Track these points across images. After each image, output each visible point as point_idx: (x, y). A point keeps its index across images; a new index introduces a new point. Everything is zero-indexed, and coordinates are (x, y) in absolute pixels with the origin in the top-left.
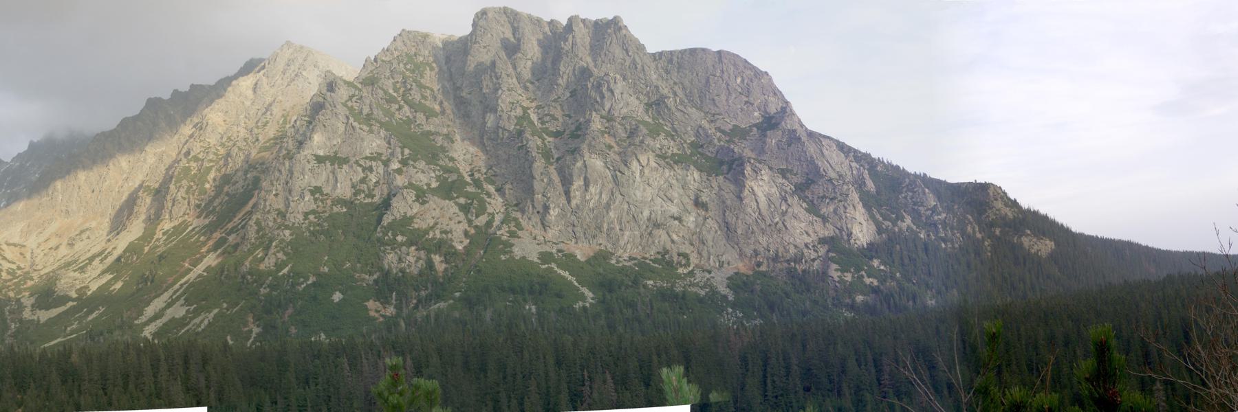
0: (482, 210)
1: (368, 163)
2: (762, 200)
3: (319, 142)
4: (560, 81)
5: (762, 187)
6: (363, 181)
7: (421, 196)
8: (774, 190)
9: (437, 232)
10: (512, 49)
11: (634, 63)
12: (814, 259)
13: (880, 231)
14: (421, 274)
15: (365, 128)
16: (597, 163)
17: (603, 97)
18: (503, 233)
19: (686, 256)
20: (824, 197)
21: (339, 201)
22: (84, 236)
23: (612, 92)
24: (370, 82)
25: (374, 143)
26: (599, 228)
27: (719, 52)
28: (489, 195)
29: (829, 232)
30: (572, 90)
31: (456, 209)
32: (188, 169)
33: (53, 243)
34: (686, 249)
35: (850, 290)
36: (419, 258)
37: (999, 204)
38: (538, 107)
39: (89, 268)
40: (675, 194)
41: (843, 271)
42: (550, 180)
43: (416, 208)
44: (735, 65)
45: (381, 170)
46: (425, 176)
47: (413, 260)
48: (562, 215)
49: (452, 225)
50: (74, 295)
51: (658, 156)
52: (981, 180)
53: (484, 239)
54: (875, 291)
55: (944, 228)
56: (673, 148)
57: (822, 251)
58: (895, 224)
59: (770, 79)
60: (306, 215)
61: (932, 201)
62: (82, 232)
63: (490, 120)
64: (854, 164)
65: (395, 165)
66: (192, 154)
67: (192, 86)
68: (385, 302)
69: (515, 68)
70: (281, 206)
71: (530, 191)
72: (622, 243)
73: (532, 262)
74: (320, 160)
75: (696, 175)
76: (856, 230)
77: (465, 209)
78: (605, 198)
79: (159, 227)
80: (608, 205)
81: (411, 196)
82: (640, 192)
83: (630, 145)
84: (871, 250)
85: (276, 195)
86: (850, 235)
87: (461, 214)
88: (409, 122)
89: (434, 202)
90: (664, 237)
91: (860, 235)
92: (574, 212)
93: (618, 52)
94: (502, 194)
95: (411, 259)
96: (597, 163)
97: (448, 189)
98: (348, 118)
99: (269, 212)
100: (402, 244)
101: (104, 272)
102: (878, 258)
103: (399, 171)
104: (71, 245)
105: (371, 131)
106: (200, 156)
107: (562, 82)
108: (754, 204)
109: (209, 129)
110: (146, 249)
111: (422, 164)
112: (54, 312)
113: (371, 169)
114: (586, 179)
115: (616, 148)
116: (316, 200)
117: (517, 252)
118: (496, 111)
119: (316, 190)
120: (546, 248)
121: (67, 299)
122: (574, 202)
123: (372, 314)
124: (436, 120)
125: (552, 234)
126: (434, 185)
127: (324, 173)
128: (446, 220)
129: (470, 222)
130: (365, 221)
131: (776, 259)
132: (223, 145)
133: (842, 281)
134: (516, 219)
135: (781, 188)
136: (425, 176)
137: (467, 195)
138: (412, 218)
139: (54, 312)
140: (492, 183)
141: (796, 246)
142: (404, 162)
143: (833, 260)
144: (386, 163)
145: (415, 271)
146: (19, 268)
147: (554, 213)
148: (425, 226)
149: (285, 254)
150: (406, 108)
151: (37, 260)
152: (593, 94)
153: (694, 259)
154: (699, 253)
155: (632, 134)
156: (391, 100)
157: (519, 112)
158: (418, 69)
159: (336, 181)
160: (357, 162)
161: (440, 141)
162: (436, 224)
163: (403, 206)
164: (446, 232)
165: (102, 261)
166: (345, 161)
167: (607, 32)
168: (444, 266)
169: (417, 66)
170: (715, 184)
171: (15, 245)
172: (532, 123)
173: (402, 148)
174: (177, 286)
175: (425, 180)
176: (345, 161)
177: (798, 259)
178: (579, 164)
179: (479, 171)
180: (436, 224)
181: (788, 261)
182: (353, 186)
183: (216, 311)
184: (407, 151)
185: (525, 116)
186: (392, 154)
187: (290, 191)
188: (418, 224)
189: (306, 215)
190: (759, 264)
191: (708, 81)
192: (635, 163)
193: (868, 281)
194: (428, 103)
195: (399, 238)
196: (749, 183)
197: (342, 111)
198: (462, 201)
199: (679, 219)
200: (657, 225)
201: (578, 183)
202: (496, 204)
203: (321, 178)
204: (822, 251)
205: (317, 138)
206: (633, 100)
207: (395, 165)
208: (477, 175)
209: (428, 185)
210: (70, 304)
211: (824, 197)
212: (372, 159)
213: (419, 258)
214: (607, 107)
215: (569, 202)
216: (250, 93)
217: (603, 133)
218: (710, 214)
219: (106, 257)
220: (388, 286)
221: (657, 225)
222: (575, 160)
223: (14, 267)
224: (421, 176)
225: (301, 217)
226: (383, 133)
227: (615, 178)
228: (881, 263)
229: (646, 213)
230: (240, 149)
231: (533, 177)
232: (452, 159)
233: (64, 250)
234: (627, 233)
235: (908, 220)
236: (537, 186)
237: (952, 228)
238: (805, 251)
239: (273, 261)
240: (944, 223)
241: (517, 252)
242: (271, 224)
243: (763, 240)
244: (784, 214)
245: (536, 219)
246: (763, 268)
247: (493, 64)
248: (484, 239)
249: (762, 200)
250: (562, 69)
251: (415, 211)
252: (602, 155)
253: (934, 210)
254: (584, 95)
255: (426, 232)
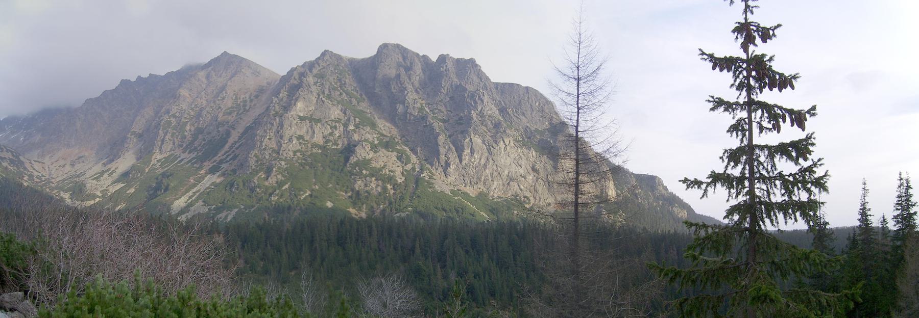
1: (334, 124)
3: (300, 108)
4: (442, 90)
6: (331, 134)
17: (476, 103)
19: (528, 198)
21: (315, 146)
22: (81, 160)
23: (482, 101)
26: (479, 179)
27: (527, 88)
30: (435, 98)
32: (169, 123)
33: (62, 162)
34: (528, 194)
36: (378, 185)
39: (102, 178)
40: (523, 163)
42: (449, 147)
43: (371, 154)
45: (342, 128)
46: (372, 137)
47: (374, 186)
48: (457, 169)
49: (395, 168)
60: (295, 152)
62: (79, 158)
63: (400, 108)
65: (351, 127)
66: (171, 113)
70: (274, 146)
71: (437, 154)
72: (493, 188)
74: (302, 119)
78: (483, 162)
79: (154, 157)
80: (485, 166)
81: (368, 147)
83: (497, 132)
85: (270, 139)
89: (383, 152)
90: (516, 186)
94: (415, 153)
96: (477, 140)
98: (319, 95)
99: (265, 149)
100: (366, 176)
104: (73, 165)
106: (177, 114)
107: (444, 91)
109: (181, 98)
110: (147, 170)
113: (335, 127)
114: (471, 149)
116: (300, 143)
118: (404, 103)
119: (300, 137)
121: (94, 197)
122: (464, 162)
127: (305, 126)
132: (192, 109)
138: (370, 160)
142: (357, 126)
144: (346, 125)
147: (452, 167)
149: (283, 176)
151: (52, 172)
152: (469, 100)
153: (532, 202)
154: (535, 198)
157: (419, 105)
159: (314, 132)
162: (385, 166)
163: (363, 153)
165: (110, 175)
167: (467, 67)
173: (355, 118)
174: (191, 193)
176: (319, 121)
178: (467, 140)
180: (385, 166)
183: (236, 210)
184: (357, 120)
186: (349, 120)
187: (281, 137)
188: (374, 164)
189: (295, 152)
191: (520, 102)
192: (502, 143)
195: (364, 172)
199: (524, 177)
200: (512, 179)
201: (467, 151)
203: (303, 130)
207: (351, 127)
210: (97, 200)
212: (336, 122)
213: (378, 185)
215: (461, 161)
216: (204, 80)
219: (112, 173)
221: (512, 179)
222: (465, 138)
225: (291, 154)
229: (506, 172)
230: (208, 113)
233: (68, 168)
234: (496, 183)
239: (274, 180)
242: (267, 157)
250: (443, 83)
251: (371, 156)
255: (380, 170)
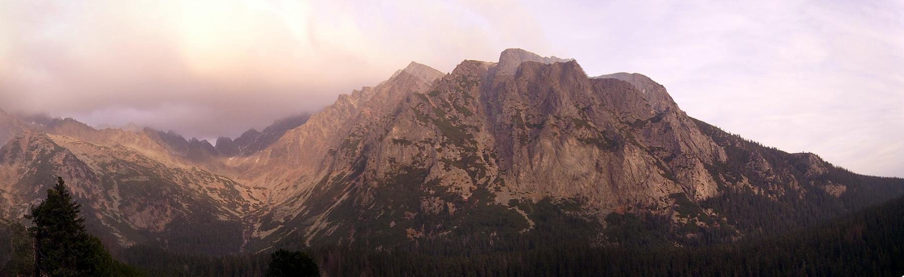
0: (482, 175)
2: (635, 168)
5: (634, 160)
6: (419, 155)
7: (448, 164)
8: (642, 162)
9: (453, 188)
10: (519, 73)
11: (579, 86)
12: (666, 207)
13: (720, 187)
14: (440, 214)
15: (423, 123)
16: (549, 144)
18: (491, 189)
20: (680, 166)
21: (406, 168)
24: (434, 94)
25: (427, 133)
28: (491, 165)
29: (678, 190)
31: (466, 174)
33: (285, 184)
35: (683, 229)
37: (815, 166)
38: (527, 110)
41: (681, 217)
44: (642, 82)
47: (437, 204)
49: (463, 185)
50: (282, 221)
51: (578, 139)
52: (807, 152)
53: (481, 193)
54: (702, 229)
55: (772, 185)
56: (589, 134)
57: (671, 203)
58: (734, 183)
59: (665, 89)
60: (386, 174)
61: (767, 166)
64: (713, 144)
67: (505, 54)
68: (418, 229)
69: (518, 86)
73: (504, 206)
74: (395, 141)
75: (597, 150)
76: (699, 189)
77: (472, 174)
81: (441, 166)
82: (570, 160)
84: (708, 203)
86: (695, 192)
87: (469, 178)
88: (454, 119)
89: (454, 170)
91: (702, 192)
92: (535, 174)
93: (572, 79)
95: (436, 204)
97: (464, 163)
101: (303, 205)
102: (711, 208)
103: (440, 150)
104: (295, 186)
105: (426, 126)
108: (629, 171)
111: (453, 146)
112: (270, 232)
113: (424, 148)
115: (559, 135)
117: (497, 200)
119: (392, 160)
120: (516, 197)
122: (534, 168)
123: (409, 236)
124: (470, 118)
125: (523, 186)
126: (459, 159)
128: (460, 181)
129: (475, 182)
130: (412, 179)
131: (639, 206)
133: (680, 223)
134: (502, 179)
135: (647, 161)
136: (453, 153)
137: (476, 166)
139: (270, 232)
140: (494, 157)
141: (653, 199)
142: (443, 145)
143: (677, 209)
144: (433, 145)
145: (437, 211)
146: (261, 203)
147: (522, 175)
148: (447, 184)
150: (454, 110)
151: (273, 198)
155: (568, 127)
156: (447, 105)
157: (514, 113)
158: (469, 85)
160: (416, 144)
161: (470, 131)
164: (458, 189)
166: (409, 143)
168: (454, 209)
169: (468, 83)
170: (607, 157)
171: (260, 188)
172: (521, 119)
175: (454, 156)
176: (409, 143)
177: (653, 208)
178: (538, 145)
179: (488, 150)
181: (647, 208)
182: (413, 159)
184: (445, 138)
185: (518, 116)
189: (386, 174)
190: (629, 209)
193: (699, 223)
194: (468, 107)
196: (626, 158)
197: (411, 112)
198: (473, 169)
201: (538, 156)
202: (493, 171)
204: (671, 203)
205: (395, 130)
206: (572, 108)
208: (487, 152)
209: (455, 159)
211: (680, 166)
212: (426, 142)
214: (558, 110)
217: (554, 126)
218: (603, 175)
220: (423, 220)
223: (258, 202)
224: (452, 153)
225: (383, 175)
226: (433, 126)
227: (557, 152)
228: (714, 211)
231: (513, 153)
232: (475, 143)
235: (746, 181)
236: (514, 158)
237: (778, 184)
238: (659, 202)
240: (773, 182)
241: (497, 200)
243: (633, 193)
244: (648, 177)
245: (514, 179)
246: (631, 211)
247: (505, 83)
248: (481, 193)
249: (635, 168)
252: (551, 139)
253: (768, 173)
254: (549, 104)
